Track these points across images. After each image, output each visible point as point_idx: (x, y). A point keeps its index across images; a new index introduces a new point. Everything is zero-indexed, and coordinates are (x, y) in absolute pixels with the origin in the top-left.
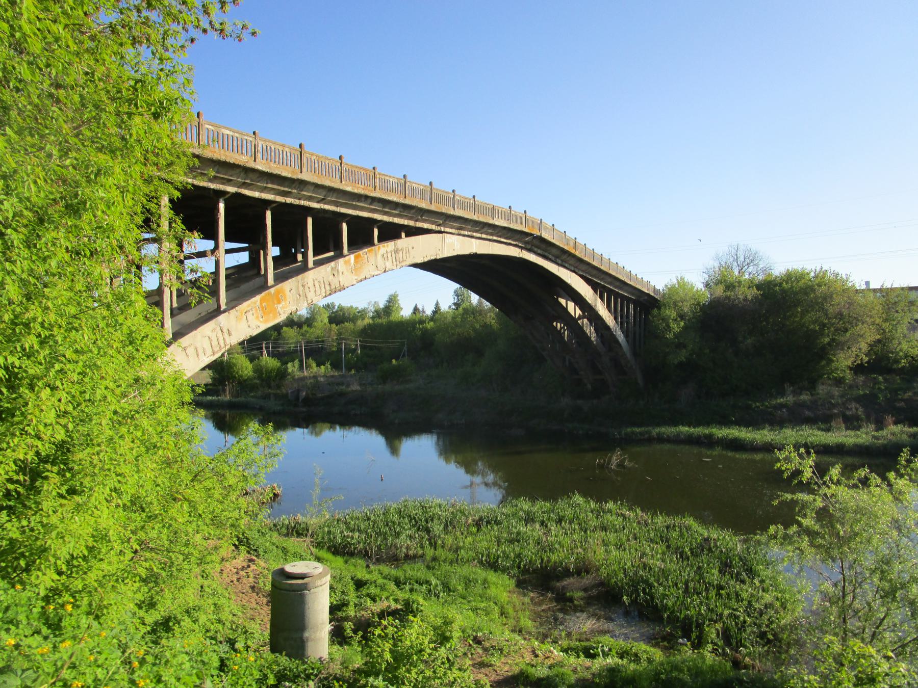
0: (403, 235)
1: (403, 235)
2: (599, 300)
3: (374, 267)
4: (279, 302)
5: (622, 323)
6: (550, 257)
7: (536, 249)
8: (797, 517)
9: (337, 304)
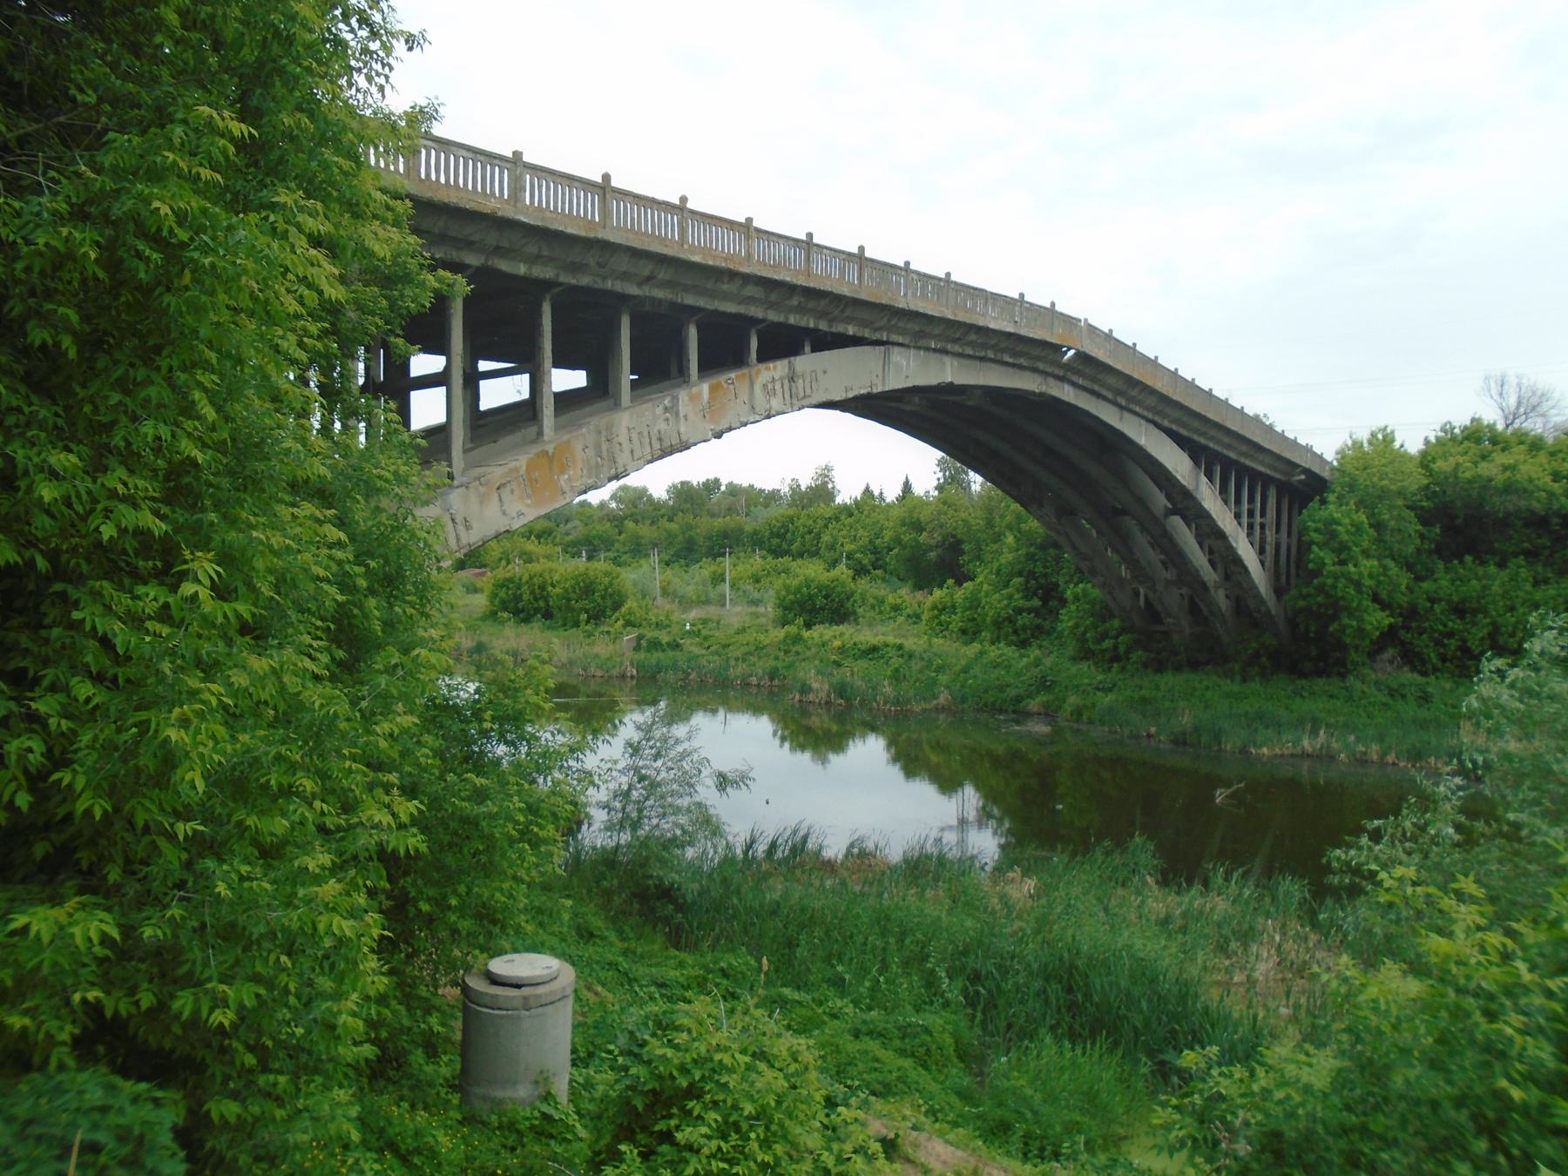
0: (807, 348)
1: (807, 348)
2: (1204, 479)
3: (747, 407)
4: (562, 472)
5: (1251, 526)
6: (1104, 392)
7: (1075, 378)
9: (724, 481)
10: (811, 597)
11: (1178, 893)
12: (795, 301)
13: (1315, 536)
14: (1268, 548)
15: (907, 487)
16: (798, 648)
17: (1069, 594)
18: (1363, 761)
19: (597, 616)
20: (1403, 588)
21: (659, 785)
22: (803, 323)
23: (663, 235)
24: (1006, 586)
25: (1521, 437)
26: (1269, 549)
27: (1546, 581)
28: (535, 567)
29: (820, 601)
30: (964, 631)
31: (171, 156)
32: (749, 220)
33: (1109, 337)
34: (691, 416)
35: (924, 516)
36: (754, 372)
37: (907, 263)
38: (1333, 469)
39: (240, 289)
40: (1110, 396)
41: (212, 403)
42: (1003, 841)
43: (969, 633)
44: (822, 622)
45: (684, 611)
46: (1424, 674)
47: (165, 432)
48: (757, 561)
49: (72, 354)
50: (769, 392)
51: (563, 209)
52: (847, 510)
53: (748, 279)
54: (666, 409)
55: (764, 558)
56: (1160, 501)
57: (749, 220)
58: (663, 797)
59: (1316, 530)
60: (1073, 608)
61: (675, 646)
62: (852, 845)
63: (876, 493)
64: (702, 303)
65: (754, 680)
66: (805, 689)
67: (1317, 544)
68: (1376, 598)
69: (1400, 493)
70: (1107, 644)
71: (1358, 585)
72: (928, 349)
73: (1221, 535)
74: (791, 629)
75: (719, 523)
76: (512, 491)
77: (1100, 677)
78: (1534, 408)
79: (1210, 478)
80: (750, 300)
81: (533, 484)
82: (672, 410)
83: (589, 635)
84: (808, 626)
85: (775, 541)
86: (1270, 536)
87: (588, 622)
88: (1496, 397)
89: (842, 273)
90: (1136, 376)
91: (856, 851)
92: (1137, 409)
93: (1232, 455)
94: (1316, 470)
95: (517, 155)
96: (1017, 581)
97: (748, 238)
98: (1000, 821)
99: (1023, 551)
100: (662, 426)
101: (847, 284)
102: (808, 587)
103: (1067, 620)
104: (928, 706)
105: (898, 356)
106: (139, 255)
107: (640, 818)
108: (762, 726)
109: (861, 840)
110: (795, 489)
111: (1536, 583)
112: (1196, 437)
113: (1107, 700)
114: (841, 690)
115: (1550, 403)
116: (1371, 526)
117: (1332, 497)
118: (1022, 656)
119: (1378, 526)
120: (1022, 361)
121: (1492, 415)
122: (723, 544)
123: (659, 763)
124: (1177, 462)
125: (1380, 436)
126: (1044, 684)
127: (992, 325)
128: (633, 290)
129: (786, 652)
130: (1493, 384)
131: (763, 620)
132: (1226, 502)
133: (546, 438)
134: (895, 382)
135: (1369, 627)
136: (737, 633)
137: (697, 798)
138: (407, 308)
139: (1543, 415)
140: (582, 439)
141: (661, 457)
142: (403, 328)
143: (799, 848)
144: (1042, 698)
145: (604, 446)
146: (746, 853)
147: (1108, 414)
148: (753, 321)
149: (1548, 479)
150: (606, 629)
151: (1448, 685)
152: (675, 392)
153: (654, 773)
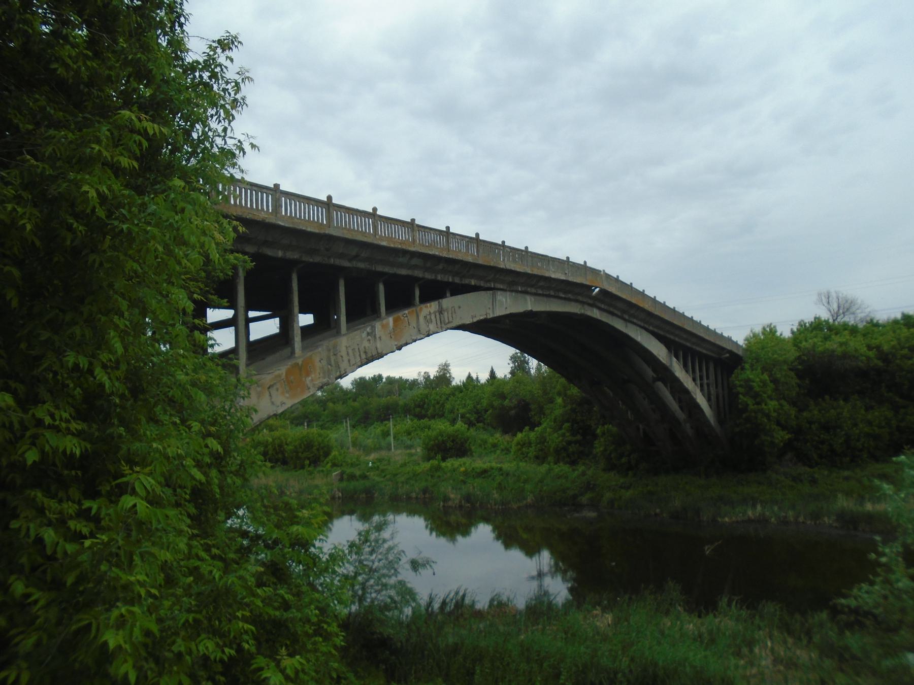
0: (448, 294)
1: (448, 294)
2: (674, 359)
3: (416, 330)
4: (308, 375)
5: (702, 386)
6: (616, 312)
7: (599, 305)
8: (346, 382)
9: (385, 375)
10: (443, 442)
11: (700, 617)
12: (441, 267)
13: (740, 389)
14: (712, 397)
15: (492, 374)
16: (439, 473)
17: (599, 431)
18: (785, 522)
19: (315, 461)
20: (793, 416)
21: (375, 571)
22: (446, 280)
23: (364, 230)
24: (560, 428)
25: (845, 326)
26: (713, 398)
27: (872, 408)
28: (276, 434)
29: (449, 444)
30: (537, 457)
31: (97, 148)
32: (413, 220)
33: (617, 280)
34: (383, 338)
35: (507, 389)
36: (418, 308)
37: (503, 242)
38: (744, 349)
39: (148, 251)
40: (619, 314)
41: (122, 340)
42: (570, 585)
43: (540, 458)
44: (451, 457)
45: (366, 455)
46: (811, 467)
47: (83, 362)
48: (409, 422)
49: (15, 303)
50: (428, 321)
51: (300, 216)
52: (458, 388)
53: (414, 254)
54: (368, 334)
55: (412, 420)
56: (650, 373)
57: (413, 220)
58: (379, 578)
59: (741, 386)
60: (602, 440)
61: (364, 477)
62: (492, 600)
63: (474, 377)
64: (387, 269)
65: (414, 495)
66: (446, 499)
67: (742, 394)
68: (778, 423)
69: (785, 362)
70: (624, 460)
71: (768, 416)
72: (517, 291)
73: (687, 392)
74: (434, 462)
75: (383, 400)
76: (277, 390)
77: (622, 480)
78: (848, 309)
79: (677, 357)
80: (415, 267)
81: (292, 383)
82: (372, 334)
83: (311, 473)
84: (444, 459)
85: (418, 410)
86: (713, 391)
87: (310, 465)
88: (826, 304)
89: (467, 249)
90: (634, 301)
91: (496, 603)
92: (635, 321)
93: (688, 344)
94: (735, 351)
95: (277, 186)
96: (567, 425)
97: (413, 230)
98: (564, 573)
99: (569, 407)
100: (366, 344)
101: (471, 256)
102: (442, 436)
103: (599, 447)
104: (521, 504)
105: (501, 297)
106: (70, 228)
107: (364, 594)
108: (418, 522)
109: (498, 595)
110: (427, 377)
111: (867, 410)
112: (668, 336)
113: (628, 494)
114: (468, 498)
115: (856, 306)
116: (771, 381)
117: (747, 366)
118: (574, 470)
119: (775, 381)
120: (570, 296)
121: (825, 315)
122: (386, 413)
123: (374, 556)
124: (658, 350)
125: (768, 329)
126: (589, 487)
127: (553, 276)
128: (346, 264)
129: (432, 476)
130: (823, 298)
131: (415, 458)
132: (687, 371)
133: (296, 355)
134: (500, 312)
135: (777, 441)
136: (401, 466)
137: (400, 578)
138: (218, 277)
139: (853, 313)
140: (319, 355)
141: (367, 363)
142: (214, 290)
143: (460, 604)
144: (589, 495)
145: (333, 358)
146: (427, 610)
147: (619, 325)
148: (417, 279)
149: (865, 349)
150: (321, 469)
151: (826, 473)
152: (373, 323)
153: (370, 564)
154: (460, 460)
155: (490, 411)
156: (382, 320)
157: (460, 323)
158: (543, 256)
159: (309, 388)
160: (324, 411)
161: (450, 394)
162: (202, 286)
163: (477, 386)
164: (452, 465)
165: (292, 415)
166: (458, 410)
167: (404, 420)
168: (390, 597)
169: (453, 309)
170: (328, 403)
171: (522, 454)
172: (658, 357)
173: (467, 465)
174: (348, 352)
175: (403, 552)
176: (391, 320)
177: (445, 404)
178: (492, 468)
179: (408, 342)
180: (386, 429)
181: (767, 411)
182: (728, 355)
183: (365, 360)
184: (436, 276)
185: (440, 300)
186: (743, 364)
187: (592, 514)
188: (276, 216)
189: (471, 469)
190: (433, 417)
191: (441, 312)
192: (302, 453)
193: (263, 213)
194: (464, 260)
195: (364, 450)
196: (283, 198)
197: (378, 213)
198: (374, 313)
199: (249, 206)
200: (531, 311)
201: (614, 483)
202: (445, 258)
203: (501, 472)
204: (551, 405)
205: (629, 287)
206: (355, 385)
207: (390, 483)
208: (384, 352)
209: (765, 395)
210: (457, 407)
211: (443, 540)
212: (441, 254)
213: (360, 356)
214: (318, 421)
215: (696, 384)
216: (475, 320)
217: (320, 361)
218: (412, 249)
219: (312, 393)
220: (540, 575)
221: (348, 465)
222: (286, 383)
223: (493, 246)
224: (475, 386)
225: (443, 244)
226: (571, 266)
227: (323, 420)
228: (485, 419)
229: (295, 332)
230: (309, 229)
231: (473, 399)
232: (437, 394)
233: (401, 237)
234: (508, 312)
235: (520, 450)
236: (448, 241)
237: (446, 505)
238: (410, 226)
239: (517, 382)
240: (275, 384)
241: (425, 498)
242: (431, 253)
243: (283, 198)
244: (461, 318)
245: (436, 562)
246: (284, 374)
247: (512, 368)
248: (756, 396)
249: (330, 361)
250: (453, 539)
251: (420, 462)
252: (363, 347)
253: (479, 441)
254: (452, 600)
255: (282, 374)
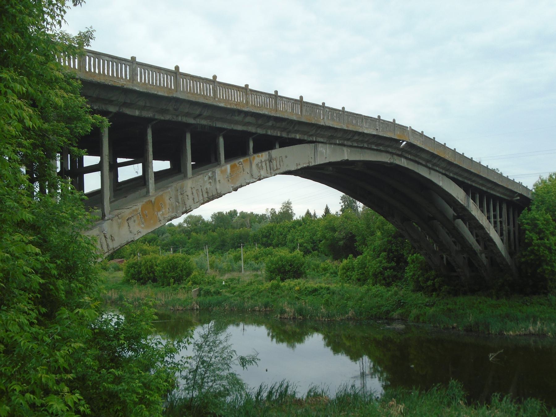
0: (277, 146)
1: (277, 146)
2: (471, 201)
3: (249, 175)
4: (159, 210)
5: (495, 223)
6: (421, 161)
7: (407, 155)
9: (239, 211)
10: (283, 266)
12: (270, 124)
14: (504, 232)
15: (327, 211)
16: (278, 291)
21: (212, 365)
22: (275, 134)
24: (378, 257)
28: (148, 257)
29: (287, 268)
30: (359, 280)
33: (422, 135)
34: (222, 181)
35: (336, 224)
36: (252, 158)
38: (533, 194)
40: (424, 163)
43: (362, 281)
44: (289, 278)
45: (221, 275)
48: (257, 250)
50: (260, 168)
51: (153, 82)
52: (298, 222)
53: (247, 114)
54: (210, 178)
55: (260, 248)
56: (451, 212)
59: (527, 224)
62: (310, 391)
63: (312, 214)
64: (225, 126)
65: (257, 308)
66: (283, 312)
67: (528, 230)
70: (429, 283)
72: (335, 144)
73: (481, 227)
74: (275, 282)
75: (237, 231)
76: (134, 221)
77: (427, 300)
80: (249, 124)
82: (213, 178)
83: (175, 289)
84: (283, 280)
85: (265, 239)
86: (505, 227)
87: (174, 283)
89: (293, 109)
91: (312, 394)
92: (437, 169)
93: (484, 189)
95: (133, 58)
96: (384, 254)
97: (246, 94)
99: (386, 239)
100: (208, 186)
101: (295, 115)
102: (282, 261)
103: (409, 272)
104: (343, 318)
105: (321, 148)
112: (466, 181)
114: (300, 311)
117: (533, 207)
118: (388, 291)
120: (381, 148)
123: (212, 353)
124: (458, 193)
126: (400, 304)
127: (366, 131)
128: (191, 121)
129: (272, 294)
131: (260, 278)
132: (483, 211)
133: (151, 194)
134: (320, 161)
136: (248, 285)
137: (231, 371)
138: (79, 132)
141: (208, 201)
143: (283, 394)
144: (399, 311)
145: (180, 197)
146: (257, 398)
147: (424, 172)
148: (250, 134)
152: (214, 169)
154: (296, 280)
155: (323, 241)
156: (221, 167)
157: (287, 170)
158: (357, 114)
159: (160, 221)
160: (189, 239)
161: (291, 227)
162: (66, 140)
163: (314, 220)
164: (289, 284)
165: (163, 242)
166: (297, 240)
167: (253, 248)
168: (223, 386)
169: (281, 158)
170: (192, 233)
171: (347, 276)
172: (457, 198)
173: (301, 285)
174: (192, 192)
175: (235, 351)
176: (228, 166)
177: (287, 236)
178: (321, 288)
179: (243, 185)
180: (238, 255)
181: (549, 245)
182: (518, 198)
183: (207, 199)
184: (266, 131)
185: (270, 151)
186: (530, 206)
187: (400, 326)
188: (133, 83)
189: (304, 287)
190: (277, 246)
191: (270, 161)
192: (169, 273)
193: (122, 80)
194: (289, 118)
195: (219, 271)
196: (139, 69)
197: (218, 80)
198: (216, 161)
199: (110, 75)
200: (347, 160)
201: (420, 302)
202: (273, 116)
203: (328, 292)
204: (372, 238)
205: (432, 141)
206: (214, 218)
207: (238, 298)
208: (223, 193)
209: (547, 232)
210: (296, 237)
211: (283, 346)
212: (270, 114)
213: (203, 195)
214: (184, 247)
215: (490, 222)
216: (299, 167)
217: (169, 199)
218: (246, 109)
219: (162, 224)
220: (363, 375)
221: (205, 283)
222: (142, 217)
223: (315, 107)
224: (312, 221)
225: (272, 105)
226: (383, 123)
227: (188, 247)
228: (319, 248)
229: (150, 175)
230: (160, 93)
231: (310, 231)
232: (280, 227)
233: (237, 99)
234: (327, 161)
235: (345, 273)
236: (276, 103)
237: (282, 317)
238: (244, 90)
239: (346, 218)
240: (133, 216)
241: (266, 311)
242: (261, 113)
243: (139, 69)
244: (287, 165)
245: (260, 360)
246: (140, 209)
247: (342, 206)
248: (540, 232)
249: (178, 200)
250: (293, 347)
251: (264, 282)
252: (205, 188)
253: (313, 266)
254: (277, 391)
255: (139, 208)
